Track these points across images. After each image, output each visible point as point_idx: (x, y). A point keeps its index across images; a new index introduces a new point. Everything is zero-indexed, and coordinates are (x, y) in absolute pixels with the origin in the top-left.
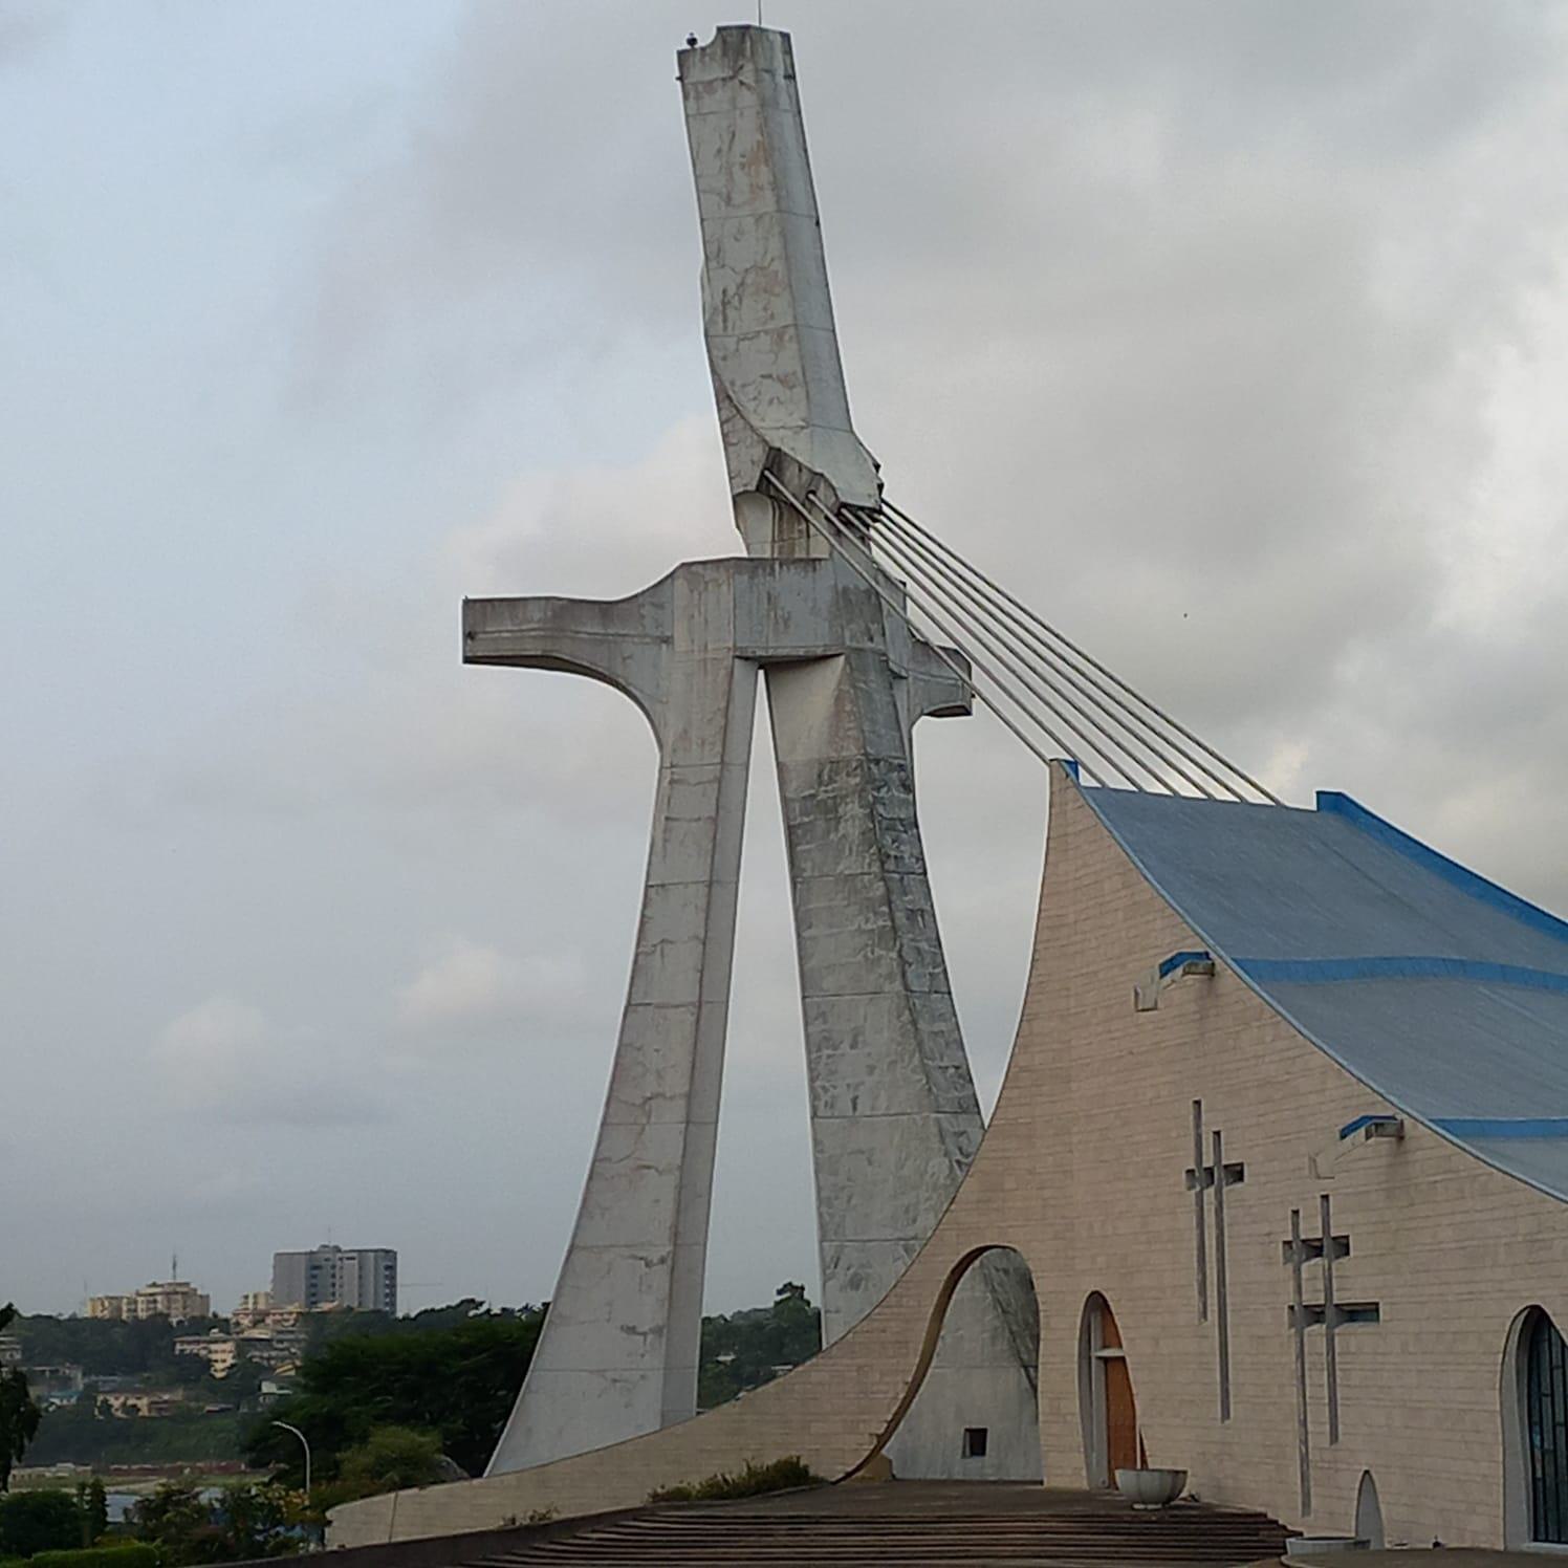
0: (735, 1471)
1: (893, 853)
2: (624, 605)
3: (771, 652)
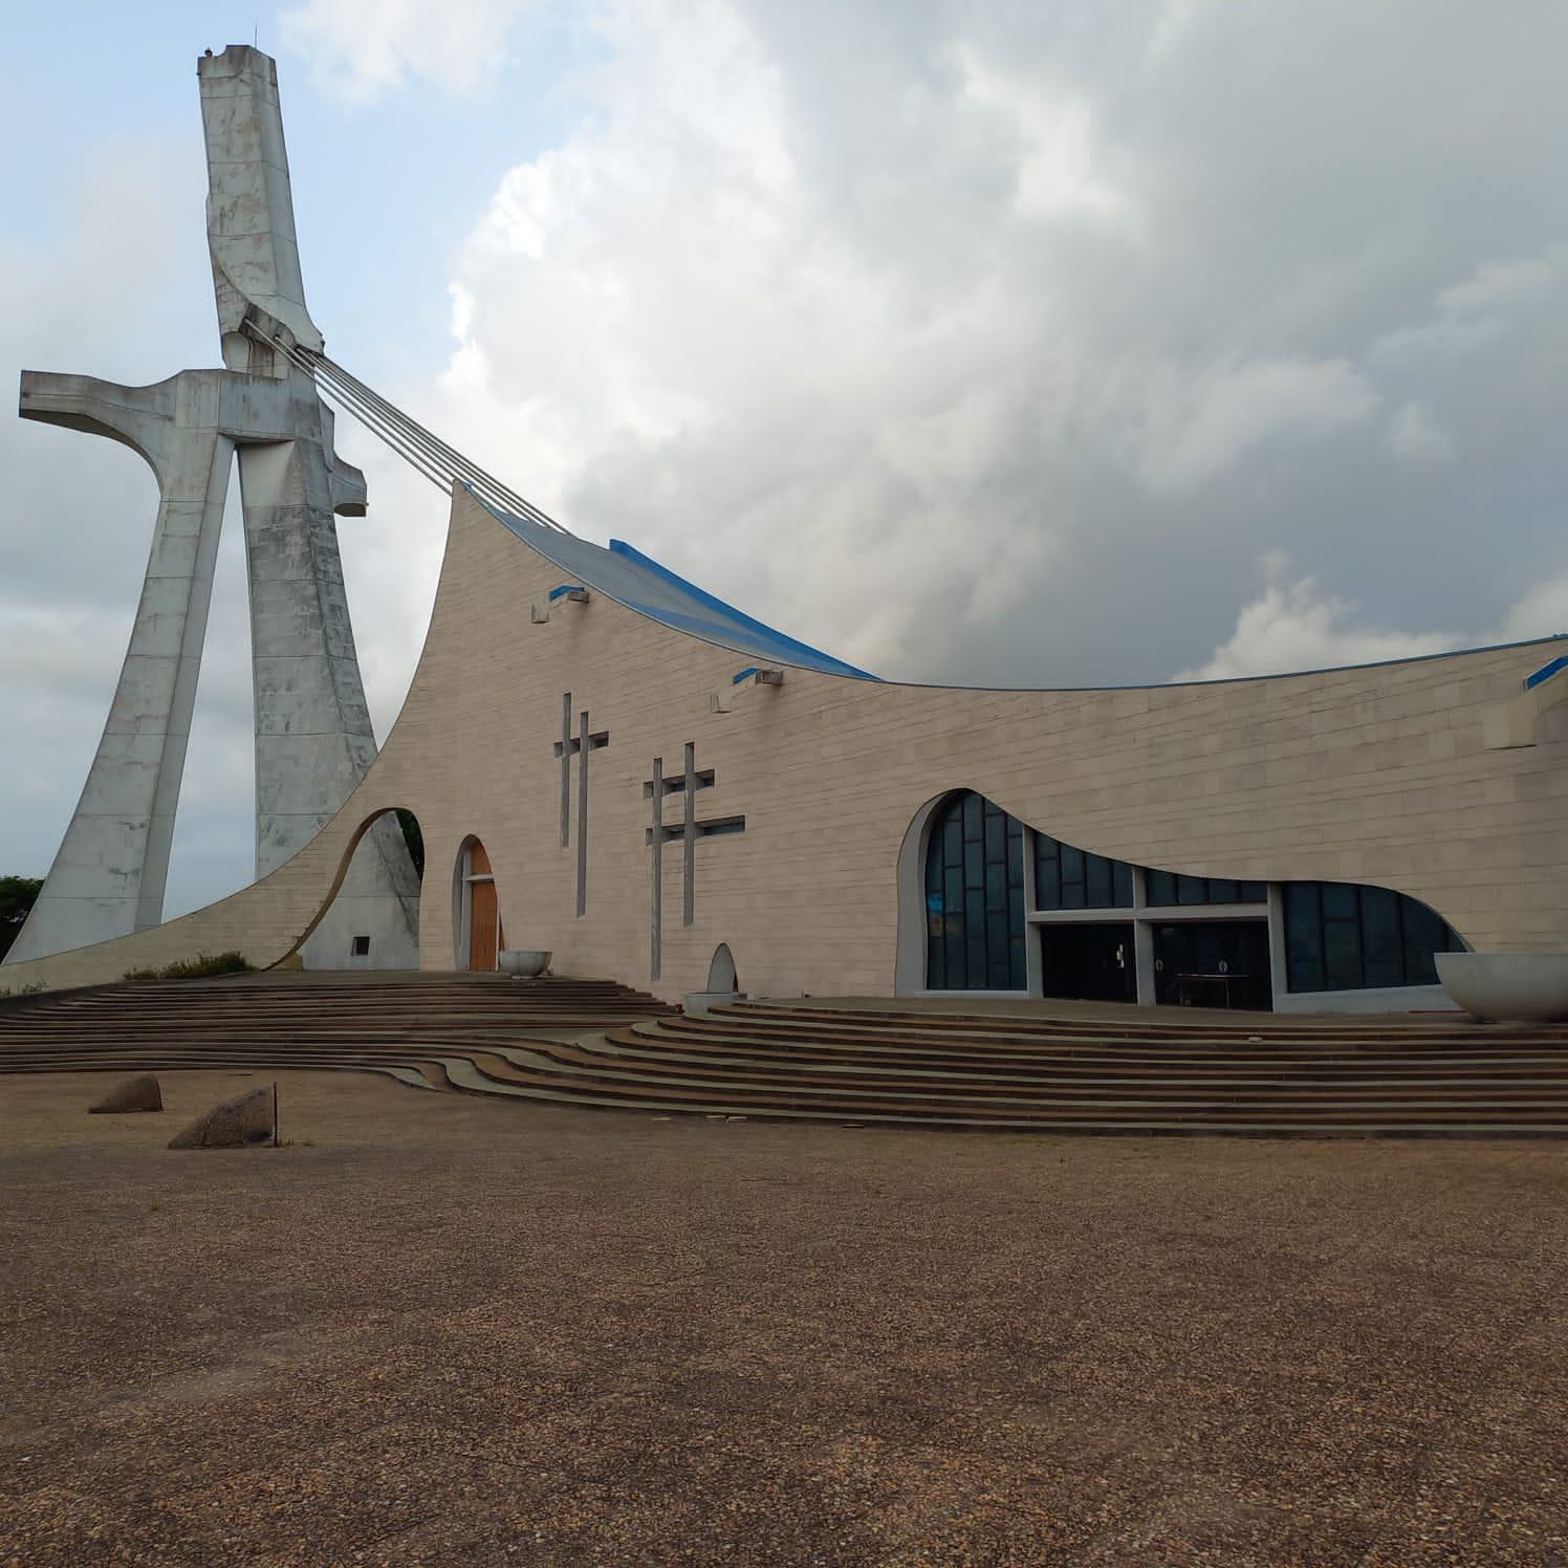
0: (191, 959)
1: (322, 568)
2: (141, 391)
3: (244, 434)
